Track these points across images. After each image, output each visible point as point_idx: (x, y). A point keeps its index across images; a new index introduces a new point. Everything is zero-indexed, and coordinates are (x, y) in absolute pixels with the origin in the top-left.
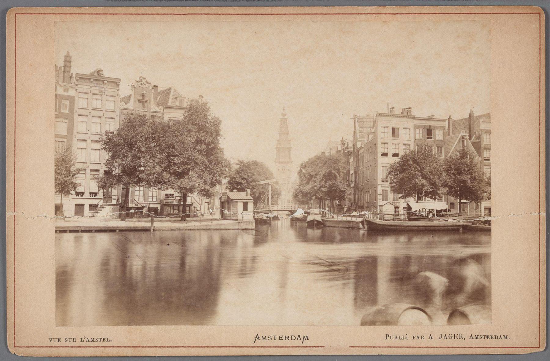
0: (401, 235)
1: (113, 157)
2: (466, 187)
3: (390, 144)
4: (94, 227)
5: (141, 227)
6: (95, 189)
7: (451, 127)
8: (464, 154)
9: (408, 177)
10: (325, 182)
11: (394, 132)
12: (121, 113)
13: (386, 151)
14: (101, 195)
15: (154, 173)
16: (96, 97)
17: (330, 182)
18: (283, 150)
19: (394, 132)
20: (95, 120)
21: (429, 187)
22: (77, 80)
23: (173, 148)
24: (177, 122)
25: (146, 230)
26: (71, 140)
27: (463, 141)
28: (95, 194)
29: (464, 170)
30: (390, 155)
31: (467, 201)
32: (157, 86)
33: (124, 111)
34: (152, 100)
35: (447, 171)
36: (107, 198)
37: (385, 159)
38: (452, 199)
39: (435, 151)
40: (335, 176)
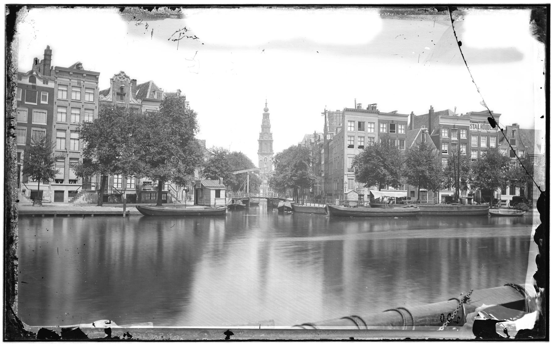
0: (365, 220)
1: (90, 147)
2: (424, 177)
3: (356, 137)
4: (70, 212)
5: (116, 212)
6: (73, 176)
7: (413, 122)
8: (423, 147)
9: (372, 168)
10: (296, 172)
11: (361, 126)
12: (100, 105)
13: (352, 143)
14: (80, 182)
15: (130, 162)
16: (74, 89)
17: (301, 172)
18: (265, 141)
19: (361, 126)
20: (74, 111)
21: (390, 177)
22: (57, 73)
23: (149, 138)
24: (153, 113)
25: (119, 215)
26: (51, 130)
27: (423, 135)
28: (75, 181)
29: (423, 161)
30: (356, 146)
31: (425, 190)
32: (136, 80)
33: (102, 103)
34: (131, 93)
35: (408, 162)
36: (86, 185)
37: (351, 151)
38: (412, 188)
39: (397, 143)
40: (306, 166)
